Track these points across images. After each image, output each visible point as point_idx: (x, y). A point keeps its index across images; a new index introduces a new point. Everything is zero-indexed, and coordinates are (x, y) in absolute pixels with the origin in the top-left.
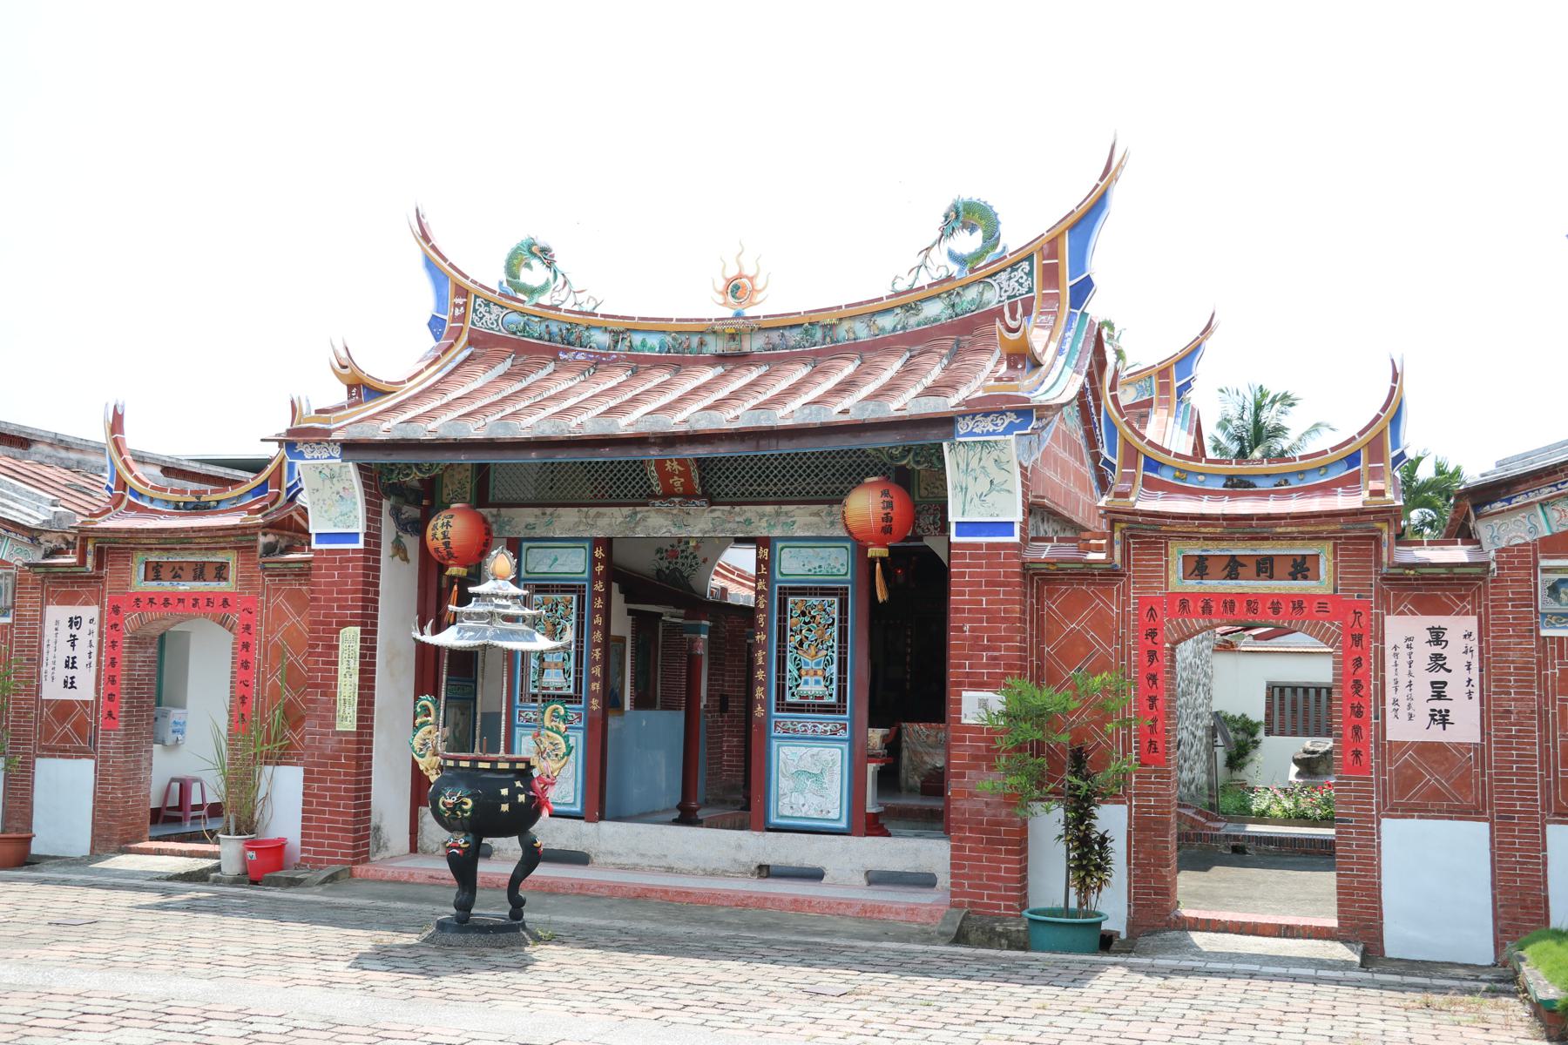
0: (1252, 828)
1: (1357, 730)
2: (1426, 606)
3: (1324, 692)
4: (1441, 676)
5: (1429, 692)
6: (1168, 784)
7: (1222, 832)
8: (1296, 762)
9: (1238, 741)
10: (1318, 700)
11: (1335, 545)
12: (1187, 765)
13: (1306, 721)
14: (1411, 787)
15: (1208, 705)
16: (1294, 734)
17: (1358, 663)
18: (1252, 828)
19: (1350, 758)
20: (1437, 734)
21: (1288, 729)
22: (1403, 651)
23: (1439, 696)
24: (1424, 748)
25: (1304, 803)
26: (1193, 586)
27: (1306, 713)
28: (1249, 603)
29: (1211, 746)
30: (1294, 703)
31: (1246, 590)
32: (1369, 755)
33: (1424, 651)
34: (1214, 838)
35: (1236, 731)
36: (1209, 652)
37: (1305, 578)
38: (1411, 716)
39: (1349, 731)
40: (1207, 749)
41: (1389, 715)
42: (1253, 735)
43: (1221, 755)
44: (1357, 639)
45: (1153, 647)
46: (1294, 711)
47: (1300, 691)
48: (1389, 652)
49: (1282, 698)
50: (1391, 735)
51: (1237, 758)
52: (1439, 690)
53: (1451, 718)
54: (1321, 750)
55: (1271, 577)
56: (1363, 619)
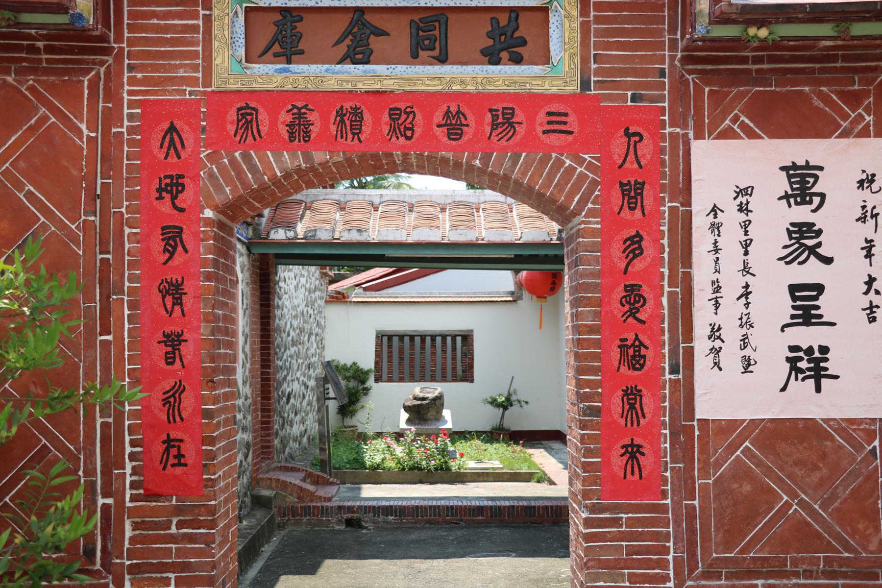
0: (371, 492)
1: (632, 396)
2: (778, 118)
3: (428, 339)
4: (810, 272)
5: (785, 308)
6: (208, 540)
7: (335, 503)
8: (407, 409)
9: (347, 388)
10: (423, 348)
12: (298, 418)
13: (412, 367)
14: (750, 520)
15: (320, 355)
16: (401, 380)
17: (634, 246)
18: (371, 492)
19: (618, 462)
20: (803, 403)
21: (396, 374)
22: (731, 218)
23: (807, 316)
24: (778, 434)
25: (418, 455)
26: (268, 76)
27: (412, 359)
28: (394, 113)
29: (323, 397)
30: (401, 351)
31: (388, 85)
32: (658, 453)
33: (774, 217)
34: (325, 511)
35: (347, 379)
37: (517, 60)
38: (748, 364)
39: (617, 402)
40: (318, 400)
41: (702, 362)
42: (363, 382)
43: (333, 406)
44: (633, 194)
45: (176, 219)
46: (401, 358)
47: (407, 339)
48: (700, 222)
49: (390, 346)
50: (707, 407)
51: (350, 404)
52: (806, 304)
53: (832, 366)
54: (431, 396)
55: (443, 59)
56: (645, 149)
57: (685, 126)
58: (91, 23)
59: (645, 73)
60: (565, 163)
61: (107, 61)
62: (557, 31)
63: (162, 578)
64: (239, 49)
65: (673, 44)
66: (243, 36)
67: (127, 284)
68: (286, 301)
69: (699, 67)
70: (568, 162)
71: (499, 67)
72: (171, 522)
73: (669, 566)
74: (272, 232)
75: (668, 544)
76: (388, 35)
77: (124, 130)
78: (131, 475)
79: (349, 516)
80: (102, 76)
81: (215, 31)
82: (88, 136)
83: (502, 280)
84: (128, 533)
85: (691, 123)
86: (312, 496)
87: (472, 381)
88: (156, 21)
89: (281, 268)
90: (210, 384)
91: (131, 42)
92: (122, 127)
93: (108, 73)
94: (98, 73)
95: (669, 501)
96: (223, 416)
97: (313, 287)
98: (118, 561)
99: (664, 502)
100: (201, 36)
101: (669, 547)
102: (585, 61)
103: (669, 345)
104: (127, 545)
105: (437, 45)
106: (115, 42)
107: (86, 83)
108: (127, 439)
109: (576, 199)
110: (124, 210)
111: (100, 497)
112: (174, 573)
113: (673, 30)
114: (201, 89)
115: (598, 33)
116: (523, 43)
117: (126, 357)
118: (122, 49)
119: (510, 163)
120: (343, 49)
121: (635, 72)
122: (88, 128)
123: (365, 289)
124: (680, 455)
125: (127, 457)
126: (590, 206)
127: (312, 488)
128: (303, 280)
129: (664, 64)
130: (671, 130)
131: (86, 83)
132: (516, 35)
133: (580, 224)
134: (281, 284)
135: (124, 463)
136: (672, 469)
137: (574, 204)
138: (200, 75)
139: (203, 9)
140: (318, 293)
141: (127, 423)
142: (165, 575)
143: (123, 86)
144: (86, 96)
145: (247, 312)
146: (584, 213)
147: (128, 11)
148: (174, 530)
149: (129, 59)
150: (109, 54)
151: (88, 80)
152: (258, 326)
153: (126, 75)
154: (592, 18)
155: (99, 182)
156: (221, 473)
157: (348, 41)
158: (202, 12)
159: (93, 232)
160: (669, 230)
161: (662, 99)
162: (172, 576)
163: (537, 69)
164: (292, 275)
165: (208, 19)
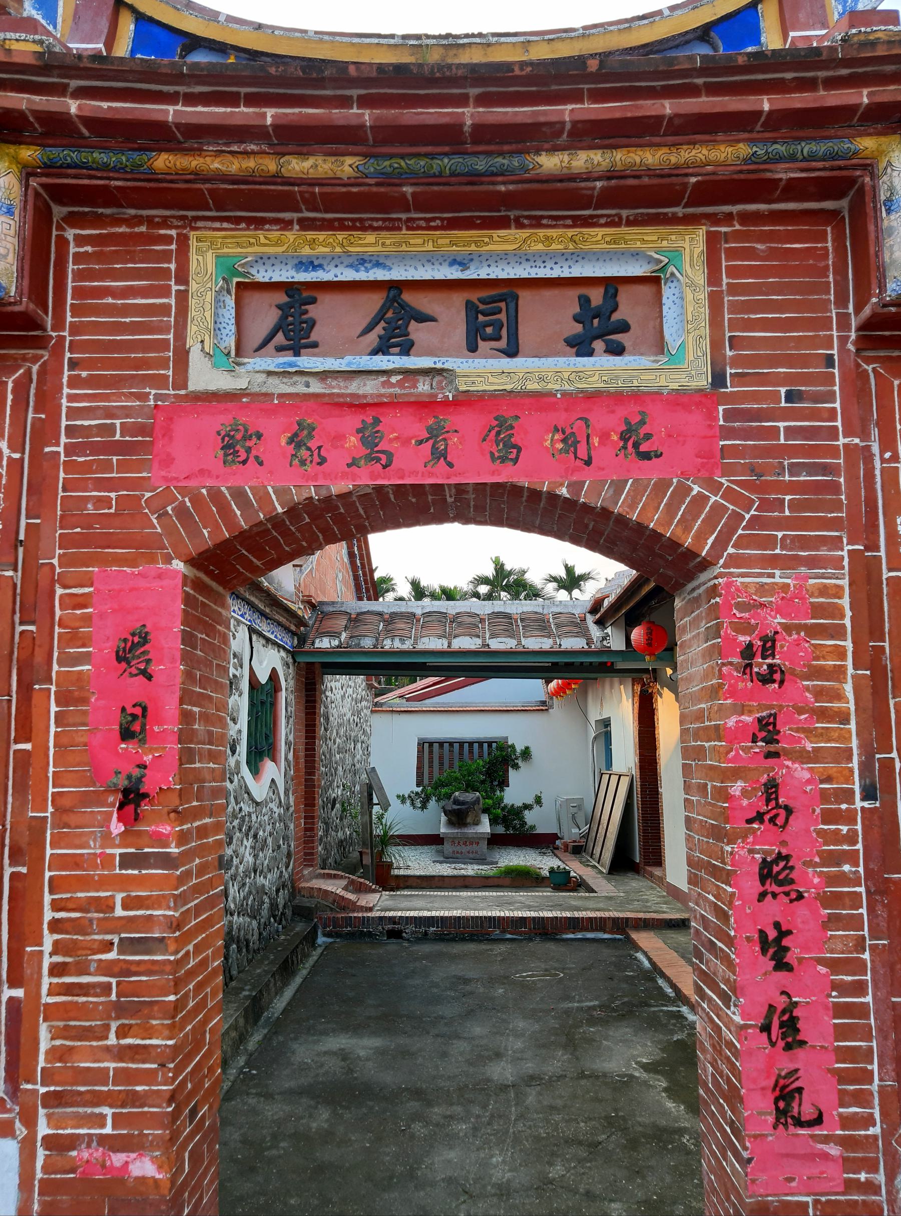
11: (712, 241)
15: (366, 761)
26: (257, 372)
36: (368, 712)
37: (617, 350)
46: (441, 764)
47: (446, 746)
55: (512, 352)
57: (865, 435)
58: (12, 294)
59: (805, 361)
60: (691, 489)
61: (42, 356)
62: (673, 307)
63: (93, 1114)
64: (227, 339)
65: (844, 320)
66: (233, 321)
67: (55, 667)
68: (334, 712)
69: (882, 353)
70: (696, 489)
71: (591, 359)
72: (107, 1027)
73: (872, 1102)
74: (317, 641)
75: (869, 1067)
76: (432, 319)
77: (61, 449)
78: (51, 955)
79: (390, 926)
80: (35, 377)
81: (193, 313)
82: (9, 458)
83: (533, 689)
84: (44, 1044)
85: (875, 432)
86: (354, 907)
87: (421, 744)
88: (110, 300)
89: (327, 678)
90: (172, 815)
91: (75, 329)
92: (58, 445)
93: (42, 372)
94: (29, 372)
95: (869, 999)
96: (197, 861)
97: (359, 697)
98: (29, 1086)
99: (862, 1000)
100: (172, 319)
101: (872, 1071)
102: (716, 345)
103: (859, 755)
104: (42, 1063)
105: (504, 332)
106: (52, 330)
107: (10, 386)
108: (47, 898)
109: (710, 541)
110: (55, 561)
111: (6, 986)
112: (111, 1106)
113: (842, 301)
114: (172, 392)
115: (735, 308)
116: (624, 327)
117: (50, 775)
118: (62, 339)
119: (611, 492)
120: (373, 338)
121: (789, 361)
122: (9, 447)
123: (408, 700)
124: (883, 924)
125: (45, 926)
126: (731, 550)
127: (351, 897)
128: (350, 691)
129: (832, 348)
130: (847, 440)
131: (10, 386)
132: (615, 317)
133: (716, 578)
134: (328, 693)
135: (41, 936)
136: (873, 948)
137: (707, 548)
138: (171, 373)
139: (176, 283)
140: (364, 703)
141: (48, 874)
142: (97, 1110)
143: (61, 388)
144: (9, 402)
145: (291, 720)
146: (722, 561)
147: (74, 288)
148: (112, 1040)
149: (71, 351)
150: (44, 348)
151: (13, 382)
152: (303, 734)
153: (66, 373)
154: (724, 287)
155: (23, 522)
156: (190, 947)
157: (379, 330)
158: (175, 288)
159: (10, 593)
160: (850, 585)
161: (831, 397)
162: (108, 1111)
163: (645, 361)
164: (338, 685)
165: (183, 297)
